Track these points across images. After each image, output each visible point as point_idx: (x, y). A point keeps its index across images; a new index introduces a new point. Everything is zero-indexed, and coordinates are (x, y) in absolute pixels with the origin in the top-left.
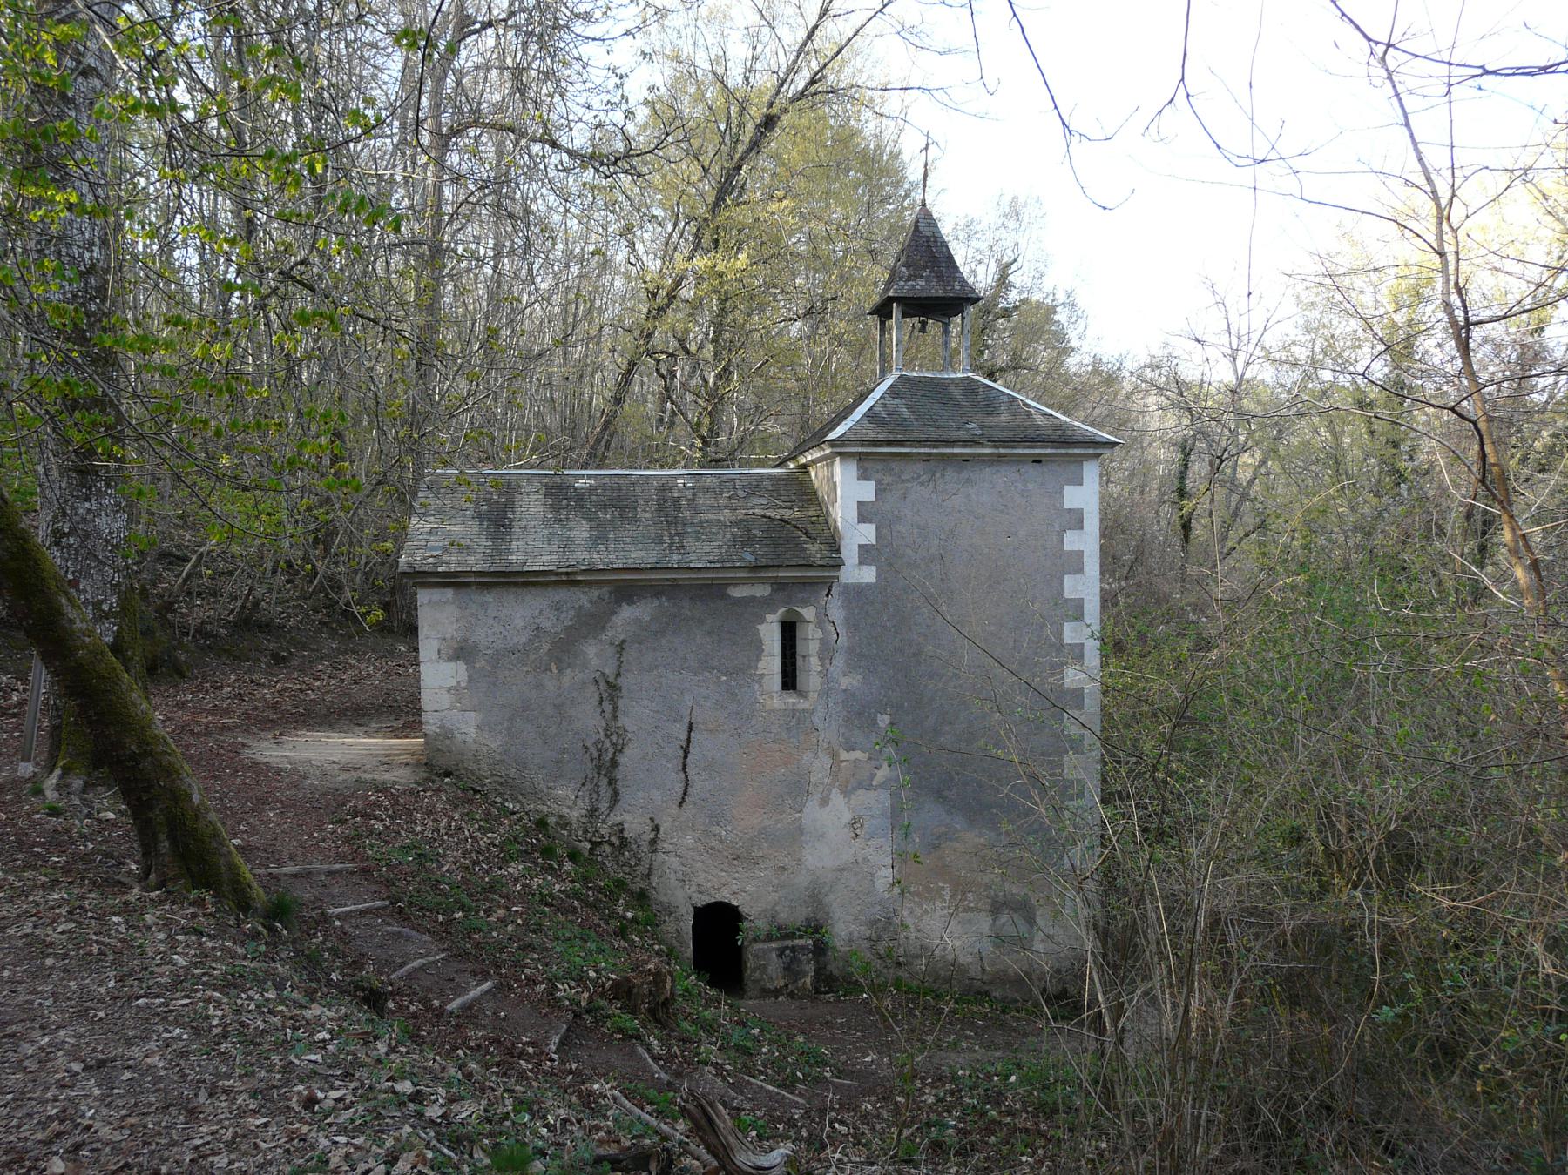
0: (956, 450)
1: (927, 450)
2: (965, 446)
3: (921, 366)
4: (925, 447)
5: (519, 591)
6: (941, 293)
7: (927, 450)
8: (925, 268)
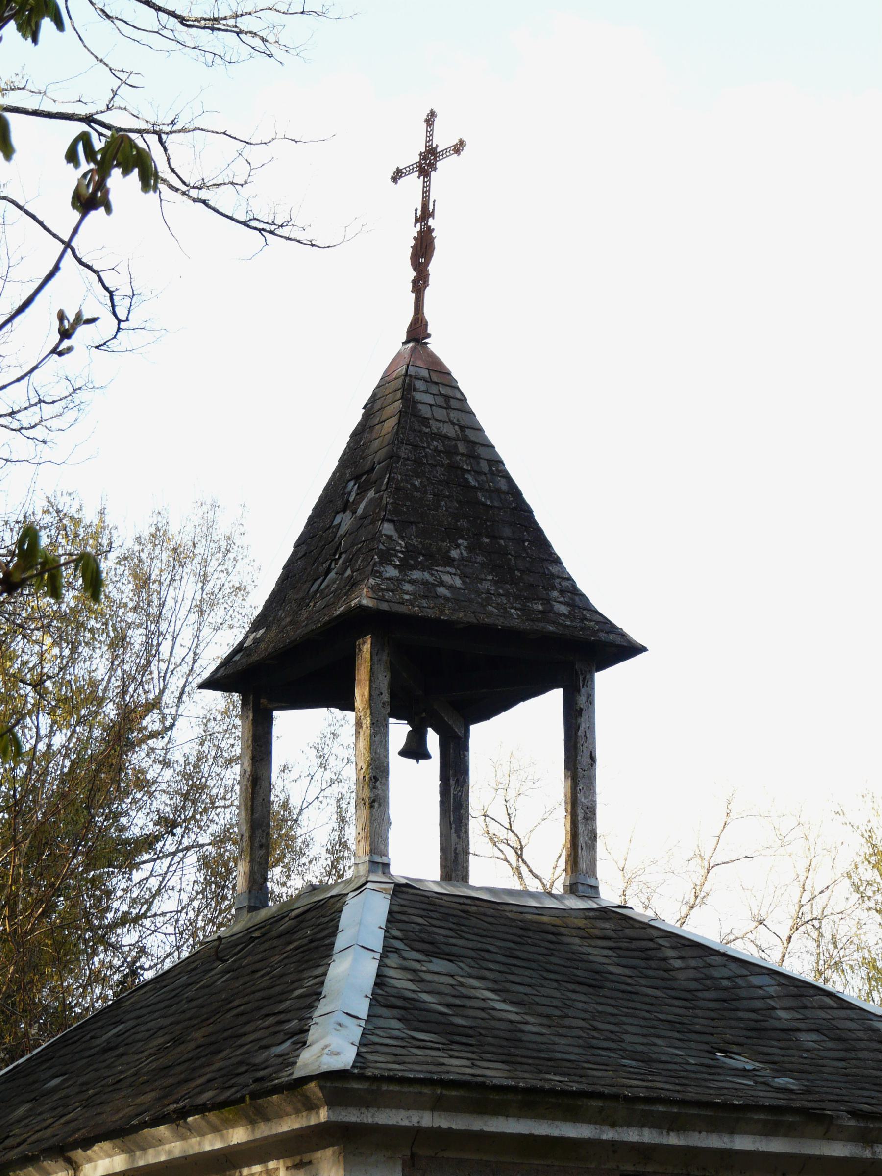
0: (743, 1143)
1: (648, 1136)
2: (770, 1130)
3: (43, 1041)
4: (642, 1123)
5: (308, 1167)
6: (515, 618)
7: (648, 1136)
8: (452, 534)
